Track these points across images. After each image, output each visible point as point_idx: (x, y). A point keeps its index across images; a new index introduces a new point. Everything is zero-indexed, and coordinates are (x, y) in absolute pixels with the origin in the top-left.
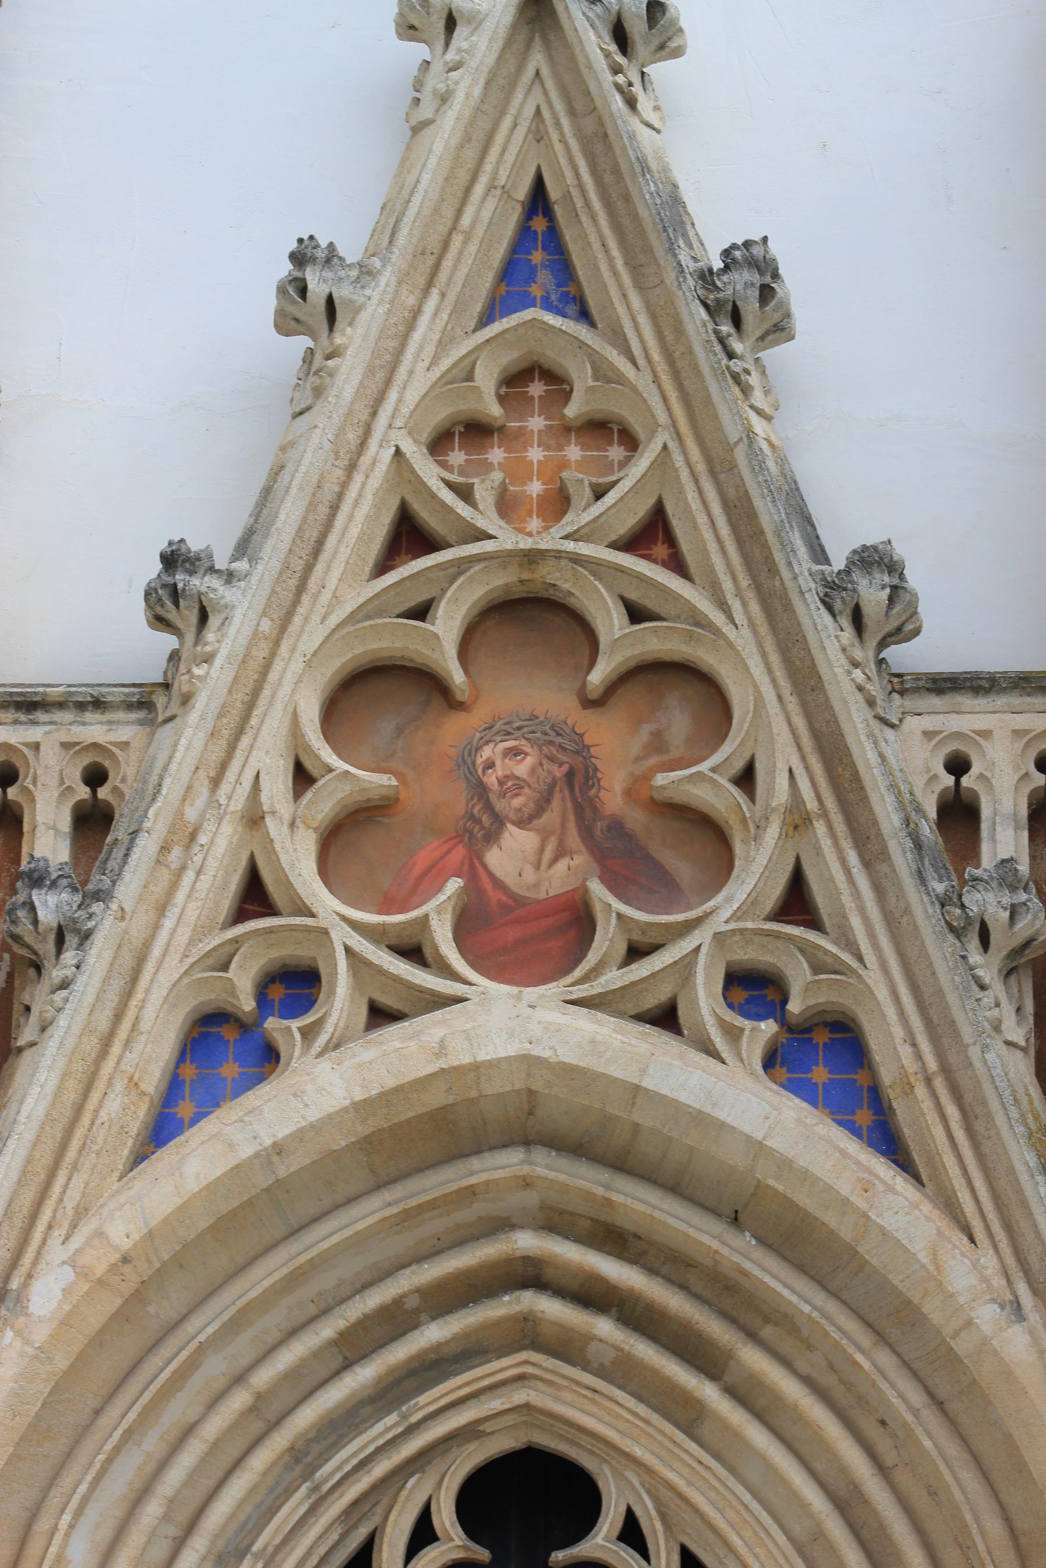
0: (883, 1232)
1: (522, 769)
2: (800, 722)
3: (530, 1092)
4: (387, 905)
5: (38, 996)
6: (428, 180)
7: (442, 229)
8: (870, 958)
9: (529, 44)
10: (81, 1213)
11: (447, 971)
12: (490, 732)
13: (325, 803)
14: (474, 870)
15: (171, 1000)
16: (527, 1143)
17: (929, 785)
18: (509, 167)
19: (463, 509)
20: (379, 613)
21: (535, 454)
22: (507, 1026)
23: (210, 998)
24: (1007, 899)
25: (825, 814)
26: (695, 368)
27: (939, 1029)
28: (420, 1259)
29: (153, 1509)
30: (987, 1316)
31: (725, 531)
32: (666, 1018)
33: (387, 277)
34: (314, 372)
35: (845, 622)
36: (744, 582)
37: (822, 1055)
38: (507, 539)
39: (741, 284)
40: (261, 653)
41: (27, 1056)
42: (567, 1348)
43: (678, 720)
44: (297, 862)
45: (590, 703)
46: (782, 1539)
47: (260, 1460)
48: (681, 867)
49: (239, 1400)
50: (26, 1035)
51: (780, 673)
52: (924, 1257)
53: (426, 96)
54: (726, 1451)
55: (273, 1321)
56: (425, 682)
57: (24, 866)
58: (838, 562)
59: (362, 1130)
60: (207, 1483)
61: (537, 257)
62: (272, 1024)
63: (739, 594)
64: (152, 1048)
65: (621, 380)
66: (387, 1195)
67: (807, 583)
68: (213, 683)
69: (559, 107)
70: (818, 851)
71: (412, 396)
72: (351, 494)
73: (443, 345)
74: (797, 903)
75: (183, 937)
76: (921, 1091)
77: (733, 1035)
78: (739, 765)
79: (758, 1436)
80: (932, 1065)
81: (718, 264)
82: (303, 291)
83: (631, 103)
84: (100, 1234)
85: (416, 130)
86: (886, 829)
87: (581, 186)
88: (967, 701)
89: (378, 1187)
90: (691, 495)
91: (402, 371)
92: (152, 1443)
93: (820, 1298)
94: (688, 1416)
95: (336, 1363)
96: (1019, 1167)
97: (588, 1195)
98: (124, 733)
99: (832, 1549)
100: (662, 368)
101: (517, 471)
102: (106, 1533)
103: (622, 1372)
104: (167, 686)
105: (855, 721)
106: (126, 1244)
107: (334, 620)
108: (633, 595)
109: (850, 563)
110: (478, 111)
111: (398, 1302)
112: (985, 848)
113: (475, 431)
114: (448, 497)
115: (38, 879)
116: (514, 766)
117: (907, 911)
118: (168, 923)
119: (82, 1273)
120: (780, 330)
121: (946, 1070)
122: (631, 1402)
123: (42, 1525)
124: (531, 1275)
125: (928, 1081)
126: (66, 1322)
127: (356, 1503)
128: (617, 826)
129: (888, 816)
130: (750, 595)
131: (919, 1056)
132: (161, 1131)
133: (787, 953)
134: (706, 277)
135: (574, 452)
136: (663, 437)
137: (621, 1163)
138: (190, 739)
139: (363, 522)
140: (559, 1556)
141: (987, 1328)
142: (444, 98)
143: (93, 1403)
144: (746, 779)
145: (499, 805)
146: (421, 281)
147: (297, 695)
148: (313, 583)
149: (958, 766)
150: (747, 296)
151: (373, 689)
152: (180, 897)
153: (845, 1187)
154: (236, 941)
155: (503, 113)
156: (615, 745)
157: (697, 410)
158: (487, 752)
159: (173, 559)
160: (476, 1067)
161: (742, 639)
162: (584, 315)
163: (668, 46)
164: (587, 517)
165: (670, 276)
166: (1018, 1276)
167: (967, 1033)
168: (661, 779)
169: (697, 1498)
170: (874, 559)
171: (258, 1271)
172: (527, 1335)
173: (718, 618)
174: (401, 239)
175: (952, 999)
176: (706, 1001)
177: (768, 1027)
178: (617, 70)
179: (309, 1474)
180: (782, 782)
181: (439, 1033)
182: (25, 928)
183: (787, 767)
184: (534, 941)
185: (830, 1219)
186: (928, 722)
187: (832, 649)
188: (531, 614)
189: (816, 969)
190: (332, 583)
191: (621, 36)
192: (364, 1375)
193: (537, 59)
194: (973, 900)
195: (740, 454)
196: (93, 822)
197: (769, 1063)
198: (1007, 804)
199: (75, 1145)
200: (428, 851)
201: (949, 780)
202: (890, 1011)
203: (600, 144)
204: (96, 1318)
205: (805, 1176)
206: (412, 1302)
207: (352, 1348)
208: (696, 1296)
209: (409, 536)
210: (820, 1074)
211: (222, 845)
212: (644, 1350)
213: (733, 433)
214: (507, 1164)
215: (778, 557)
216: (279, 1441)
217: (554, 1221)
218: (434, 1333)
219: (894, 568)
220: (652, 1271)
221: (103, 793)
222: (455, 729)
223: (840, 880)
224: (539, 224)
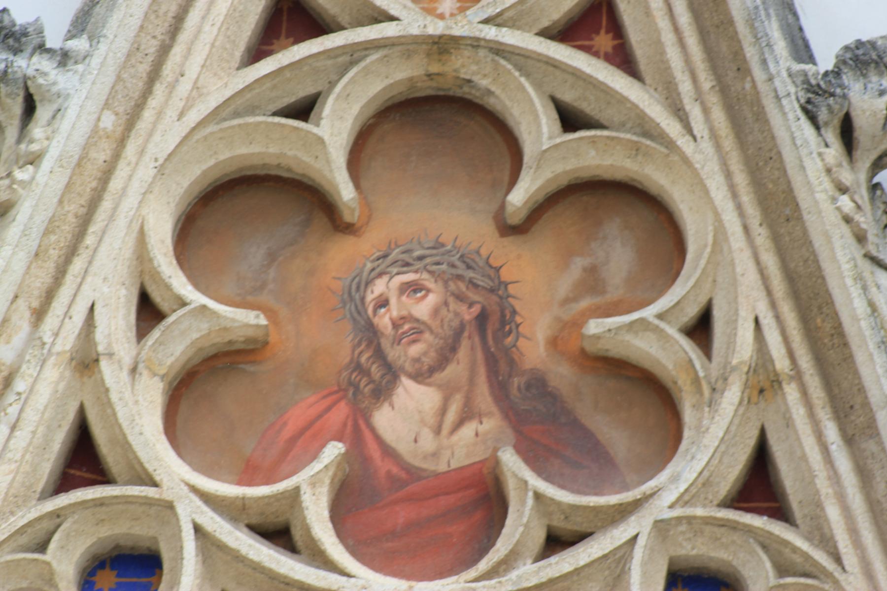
1: (423, 308)
4: (250, 473)
11: (320, 559)
12: (386, 261)
13: (175, 344)
14: (358, 434)
20: (252, 110)
25: (798, 376)
35: (832, 135)
36: (707, 82)
40: (101, 155)
43: (618, 252)
44: (138, 417)
45: (511, 230)
48: (616, 437)
51: (747, 198)
56: (306, 197)
58: (826, 61)
63: (699, 97)
70: (789, 422)
74: (760, 486)
78: (692, 311)
107: (194, 116)
109: (841, 62)
116: (411, 303)
128: (538, 384)
130: (713, 100)
144: (701, 329)
145: (393, 353)
147: (146, 207)
151: (240, 205)
154: (58, 515)
156: (539, 283)
158: (379, 287)
161: (702, 154)
168: (594, 327)
173: (671, 127)
183: (752, 315)
187: (814, 168)
189: (782, 570)
211: (44, 394)
215: (750, 52)
222: (340, 257)
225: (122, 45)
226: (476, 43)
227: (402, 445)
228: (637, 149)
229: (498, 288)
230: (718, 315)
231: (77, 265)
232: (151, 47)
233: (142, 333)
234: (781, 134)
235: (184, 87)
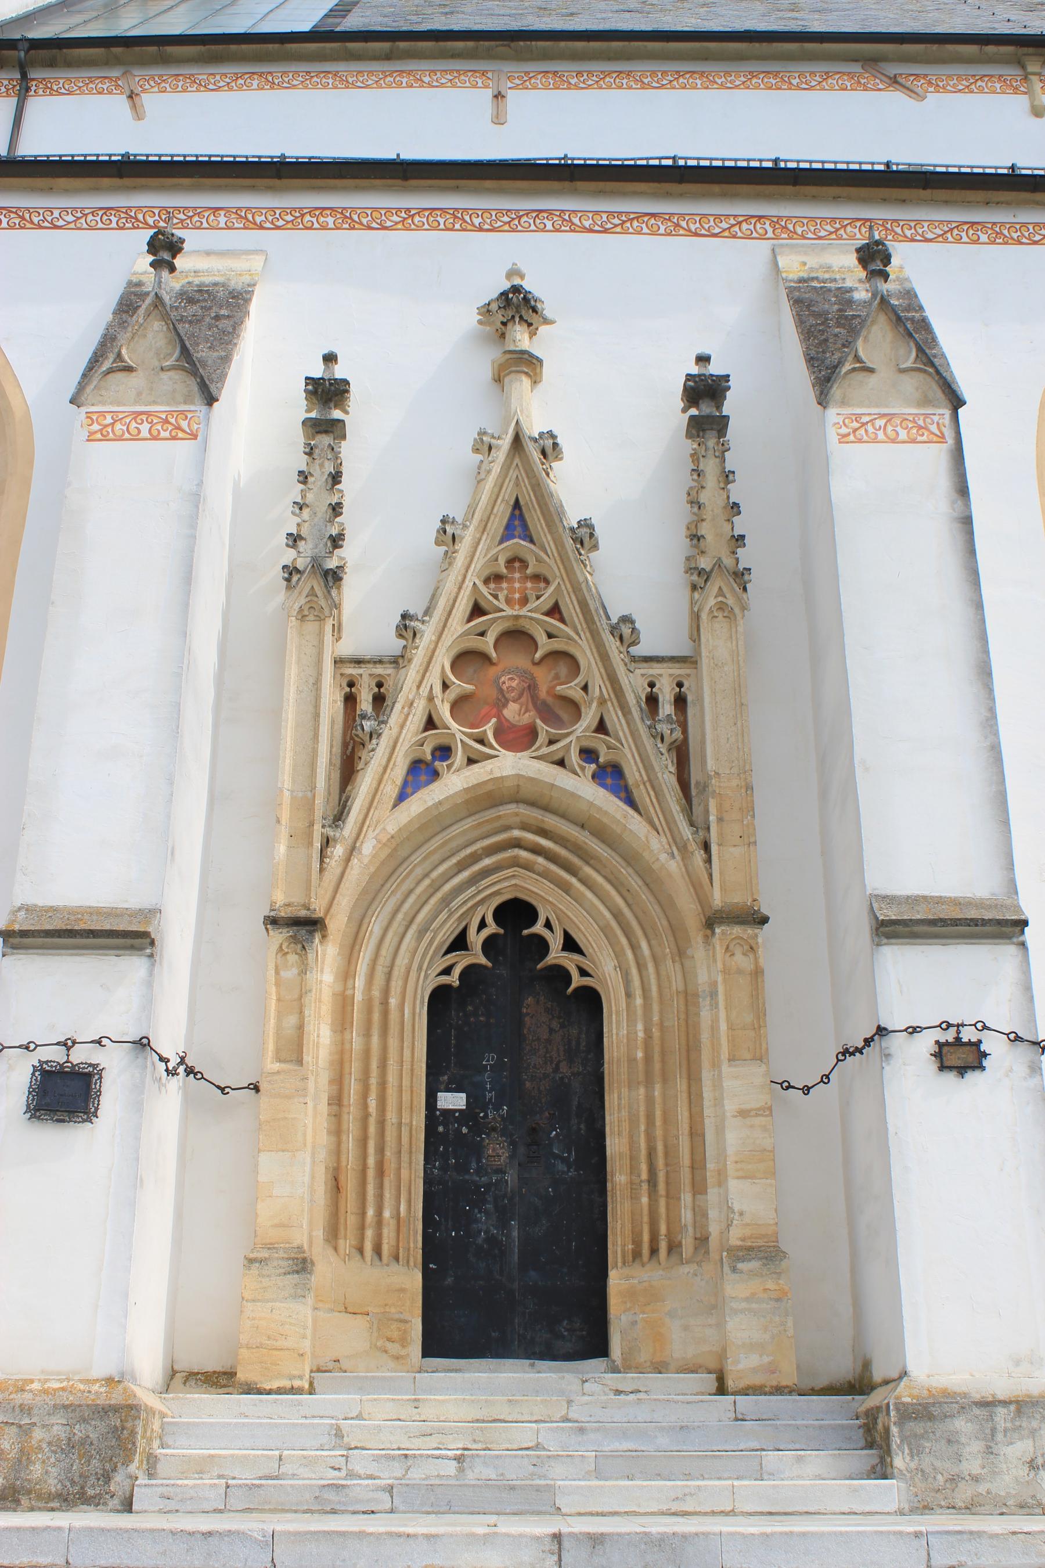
0: (631, 830)
1: (514, 684)
2: (602, 670)
3: (518, 786)
4: (472, 726)
5: (364, 754)
6: (485, 498)
7: (488, 513)
8: (625, 745)
9: (514, 455)
10: (378, 822)
11: (492, 747)
12: (504, 672)
13: (452, 694)
14: (499, 716)
15: (406, 755)
16: (517, 802)
17: (644, 691)
18: (508, 494)
19: (495, 602)
20: (469, 634)
21: (517, 585)
22: (508, 764)
23: (417, 755)
24: (670, 727)
25: (611, 699)
26: (568, 558)
27: (648, 767)
28: (483, 838)
29: (400, 916)
30: (663, 857)
31: (578, 610)
32: (561, 763)
33: (472, 528)
34: (449, 558)
35: (617, 639)
36: (585, 626)
37: (610, 775)
38: (509, 612)
39: (584, 531)
40: (432, 646)
41: (361, 773)
42: (528, 867)
43: (563, 669)
44: (444, 711)
45: (535, 664)
46: (596, 927)
47: (433, 901)
48: (565, 716)
49: (427, 882)
50: (360, 766)
51: (596, 655)
52: (644, 839)
53: (482, 471)
54: (578, 899)
55: (436, 857)
56: (482, 657)
57: (358, 712)
58: (614, 620)
59: (466, 797)
60: (416, 908)
61: (517, 523)
62: (437, 763)
63: (583, 630)
64: (399, 772)
65: (545, 562)
66: (473, 818)
67: (605, 626)
68: (419, 656)
69: (524, 475)
70: (609, 711)
71: (479, 566)
72: (460, 597)
73: (488, 550)
74: (601, 727)
75: (409, 736)
76: (642, 787)
77: (583, 769)
78: (583, 684)
79: (589, 895)
80: (645, 778)
81: (576, 526)
82: (445, 532)
83: (548, 474)
84: (384, 829)
85: (479, 482)
86: (631, 704)
87: (531, 500)
88: (655, 665)
89: (470, 815)
90: (567, 599)
91: (476, 558)
92: (399, 895)
93: (610, 851)
94: (566, 888)
95: (456, 871)
96: (674, 811)
97: (536, 818)
98: (389, 671)
99: (612, 929)
100: (558, 559)
101: (512, 590)
102: (385, 923)
103: (545, 874)
104: (403, 656)
105: (621, 671)
106: (393, 832)
107: (455, 637)
108: (549, 630)
109: (619, 620)
110: (499, 476)
111: (476, 852)
112: (661, 711)
113: (498, 578)
114: (490, 598)
115: (364, 717)
116: (511, 683)
117: (637, 730)
118: (404, 732)
119: (379, 842)
120: (595, 547)
121: (650, 780)
122: (548, 884)
123: (366, 921)
124: (517, 844)
125: (644, 784)
126: (374, 856)
127: (462, 915)
128: (544, 703)
129: (631, 700)
130: (587, 631)
131: (641, 776)
132: (402, 797)
133: (598, 742)
134: (572, 529)
135: (529, 585)
136: (558, 580)
137: (546, 809)
138: (412, 674)
139: (463, 606)
140: (525, 932)
141: (663, 861)
142: (489, 472)
143: (382, 883)
144: (585, 688)
145: (507, 695)
146: (481, 530)
147: (443, 660)
148: (448, 625)
149: (652, 685)
150: (585, 536)
151: (466, 659)
152: (408, 723)
153: (619, 816)
154: (425, 737)
155: (506, 477)
156: (543, 677)
157: (570, 572)
158: (503, 679)
159: (405, 616)
160: (502, 777)
161: (584, 644)
162: (532, 541)
163: (558, 457)
164: (535, 605)
165: (561, 529)
166: (673, 844)
167: (657, 769)
168: (558, 688)
169: (570, 914)
170: (626, 619)
171: (433, 841)
172: (515, 863)
173: (576, 637)
174: (476, 516)
175: (652, 758)
176: (574, 758)
177: (593, 766)
178: (543, 464)
179: (447, 905)
180: (597, 689)
181: (491, 766)
182: (360, 732)
183: (599, 684)
184: (520, 738)
185: (614, 827)
186: (643, 671)
187: (614, 647)
188: (516, 636)
189: (609, 748)
190: (454, 625)
191: (544, 453)
192: (465, 875)
193: (517, 460)
194: (659, 727)
195: (583, 586)
196: (379, 700)
197: (593, 777)
198: (667, 697)
199: (376, 801)
200: (485, 709)
201: (649, 689)
202: (632, 762)
203: (539, 489)
204: (383, 856)
205: (606, 813)
206: (479, 852)
207: (461, 866)
208: (570, 851)
209: (477, 610)
210: (609, 781)
211: (421, 707)
212: (553, 867)
213: (581, 579)
214: (512, 808)
215: (596, 618)
216: (439, 895)
217: (525, 827)
218: (487, 862)
219: (633, 622)
220: (556, 842)
221: (382, 690)
222: (492, 671)
223: (615, 719)
224: (517, 512)
225: (437, 619)
226: (525, 617)
227: (511, 719)
228: (567, 643)
229: (533, 678)
230: (590, 685)
231: (428, 674)
232: (443, 619)
233: (444, 691)
234: (605, 639)
235: (452, 629)
